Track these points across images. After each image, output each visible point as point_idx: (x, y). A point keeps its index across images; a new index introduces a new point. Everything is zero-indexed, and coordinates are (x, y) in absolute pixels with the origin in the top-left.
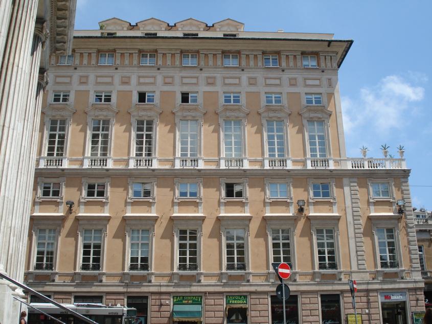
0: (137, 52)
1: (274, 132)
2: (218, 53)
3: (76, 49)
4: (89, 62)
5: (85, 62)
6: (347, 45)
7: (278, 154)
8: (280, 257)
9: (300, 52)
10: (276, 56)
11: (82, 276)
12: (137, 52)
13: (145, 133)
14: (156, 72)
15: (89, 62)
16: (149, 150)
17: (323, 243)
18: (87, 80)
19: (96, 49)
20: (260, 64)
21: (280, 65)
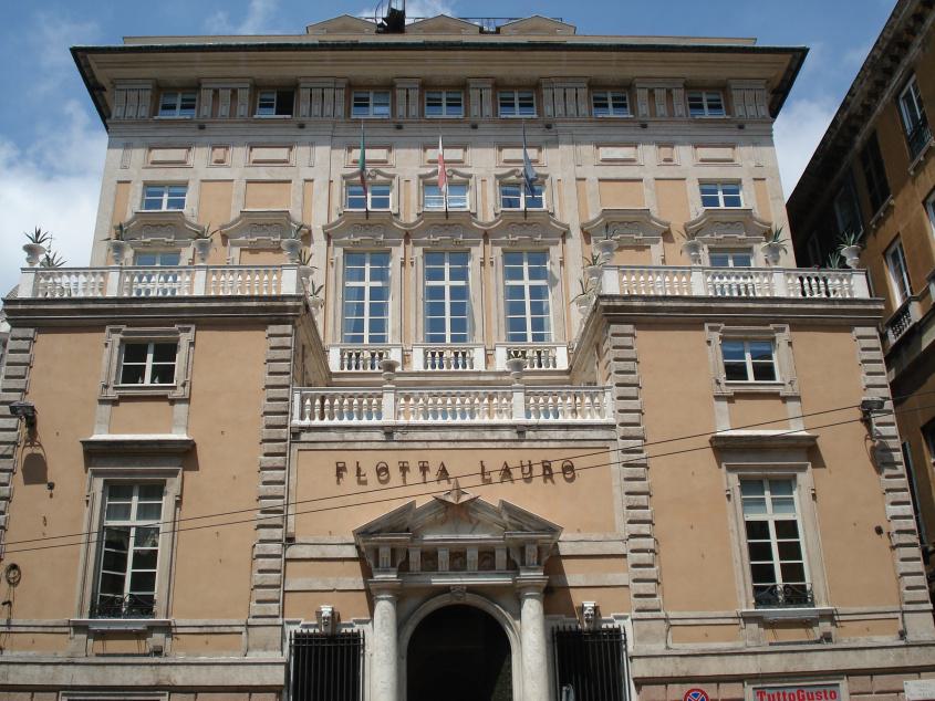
0: (150, 87)
1: (522, 278)
2: (581, 85)
3: (203, 81)
4: (233, 113)
5: (224, 110)
6: (792, 61)
7: (533, 335)
8: (781, 559)
9: (587, 80)
10: (718, 94)
11: (465, 569)
12: (150, 87)
13: (447, 283)
14: (467, 133)
15: (233, 113)
16: (538, 325)
17: (765, 524)
19: (150, 81)
20: (584, 109)
21: (540, 112)
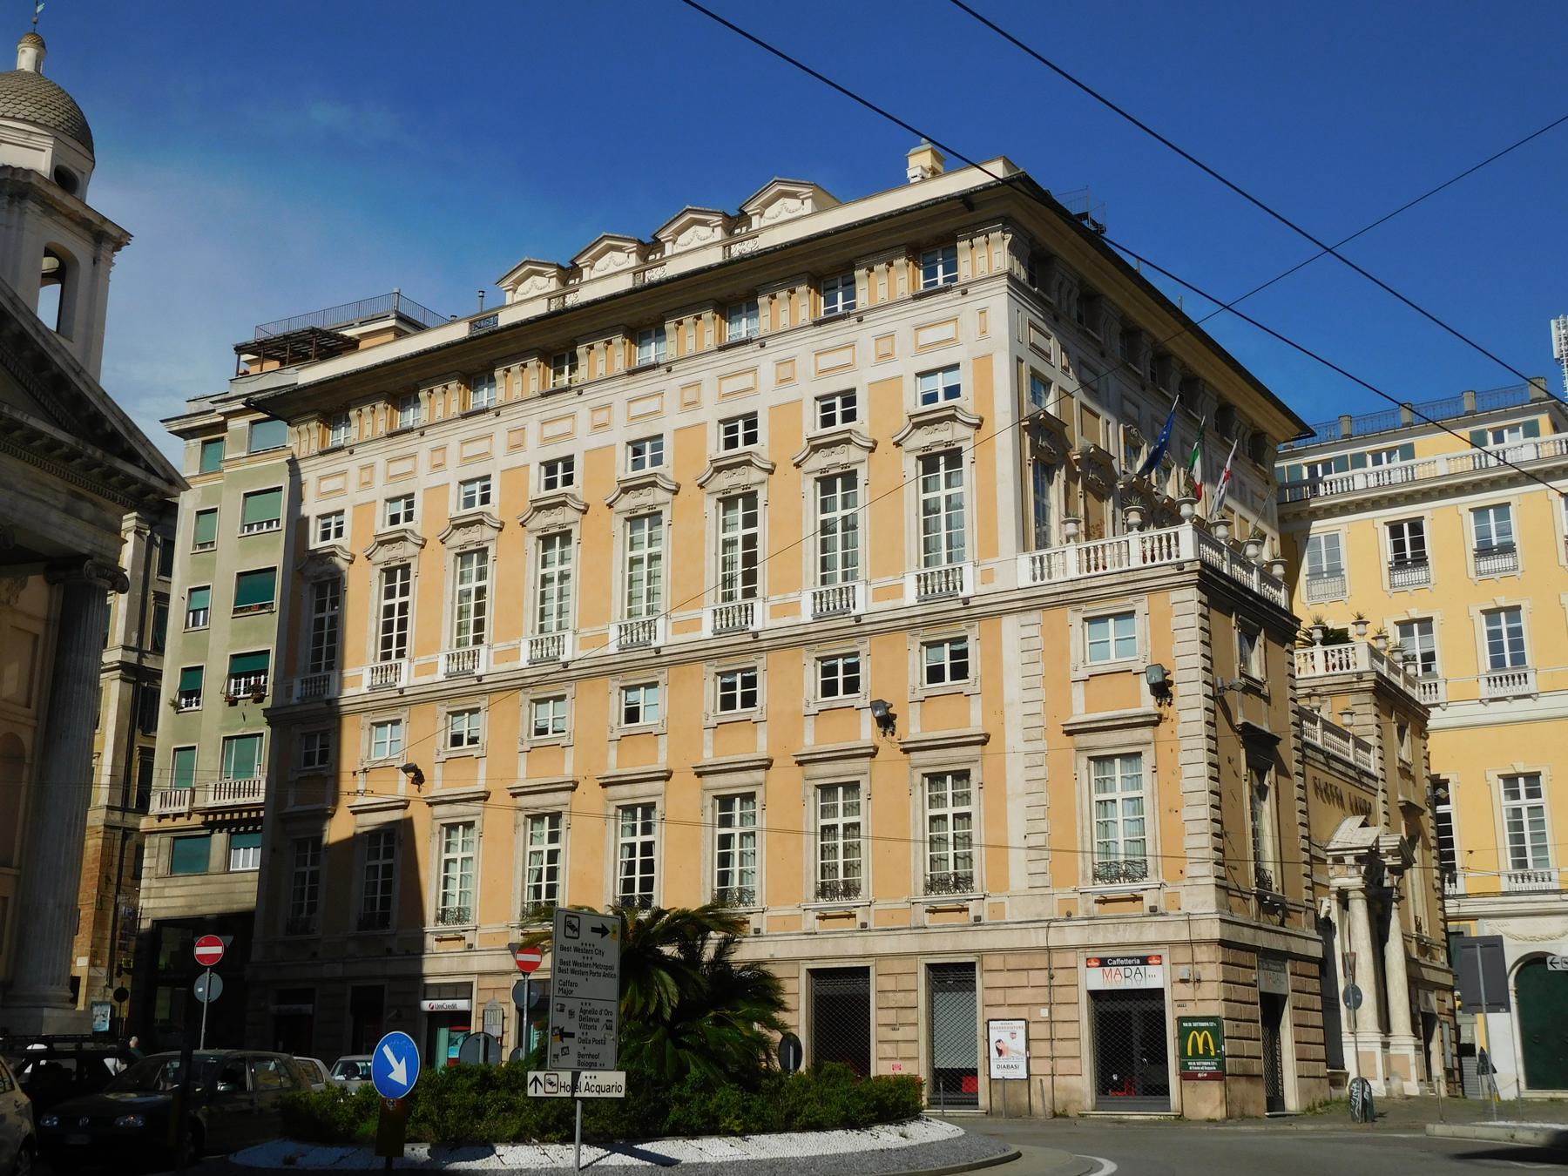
18: (523, 436)
